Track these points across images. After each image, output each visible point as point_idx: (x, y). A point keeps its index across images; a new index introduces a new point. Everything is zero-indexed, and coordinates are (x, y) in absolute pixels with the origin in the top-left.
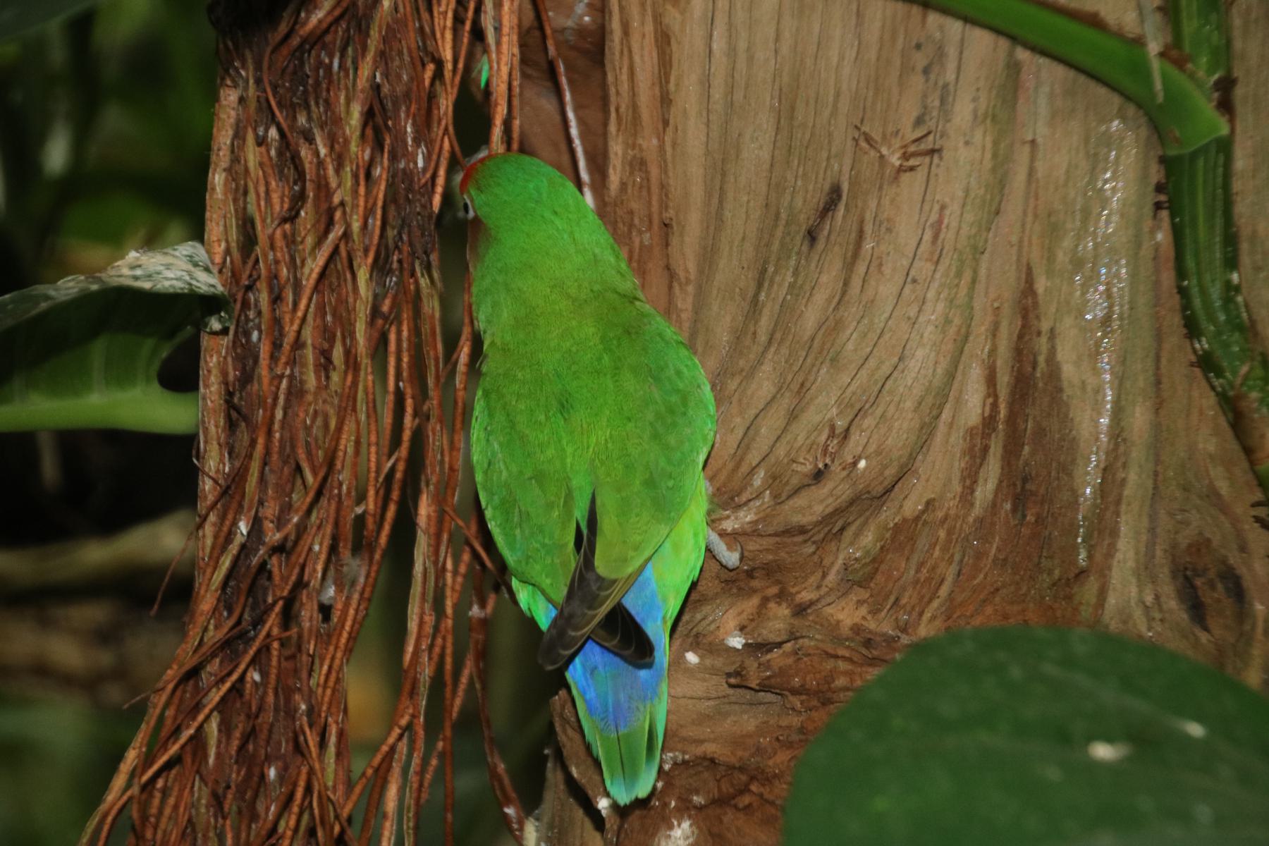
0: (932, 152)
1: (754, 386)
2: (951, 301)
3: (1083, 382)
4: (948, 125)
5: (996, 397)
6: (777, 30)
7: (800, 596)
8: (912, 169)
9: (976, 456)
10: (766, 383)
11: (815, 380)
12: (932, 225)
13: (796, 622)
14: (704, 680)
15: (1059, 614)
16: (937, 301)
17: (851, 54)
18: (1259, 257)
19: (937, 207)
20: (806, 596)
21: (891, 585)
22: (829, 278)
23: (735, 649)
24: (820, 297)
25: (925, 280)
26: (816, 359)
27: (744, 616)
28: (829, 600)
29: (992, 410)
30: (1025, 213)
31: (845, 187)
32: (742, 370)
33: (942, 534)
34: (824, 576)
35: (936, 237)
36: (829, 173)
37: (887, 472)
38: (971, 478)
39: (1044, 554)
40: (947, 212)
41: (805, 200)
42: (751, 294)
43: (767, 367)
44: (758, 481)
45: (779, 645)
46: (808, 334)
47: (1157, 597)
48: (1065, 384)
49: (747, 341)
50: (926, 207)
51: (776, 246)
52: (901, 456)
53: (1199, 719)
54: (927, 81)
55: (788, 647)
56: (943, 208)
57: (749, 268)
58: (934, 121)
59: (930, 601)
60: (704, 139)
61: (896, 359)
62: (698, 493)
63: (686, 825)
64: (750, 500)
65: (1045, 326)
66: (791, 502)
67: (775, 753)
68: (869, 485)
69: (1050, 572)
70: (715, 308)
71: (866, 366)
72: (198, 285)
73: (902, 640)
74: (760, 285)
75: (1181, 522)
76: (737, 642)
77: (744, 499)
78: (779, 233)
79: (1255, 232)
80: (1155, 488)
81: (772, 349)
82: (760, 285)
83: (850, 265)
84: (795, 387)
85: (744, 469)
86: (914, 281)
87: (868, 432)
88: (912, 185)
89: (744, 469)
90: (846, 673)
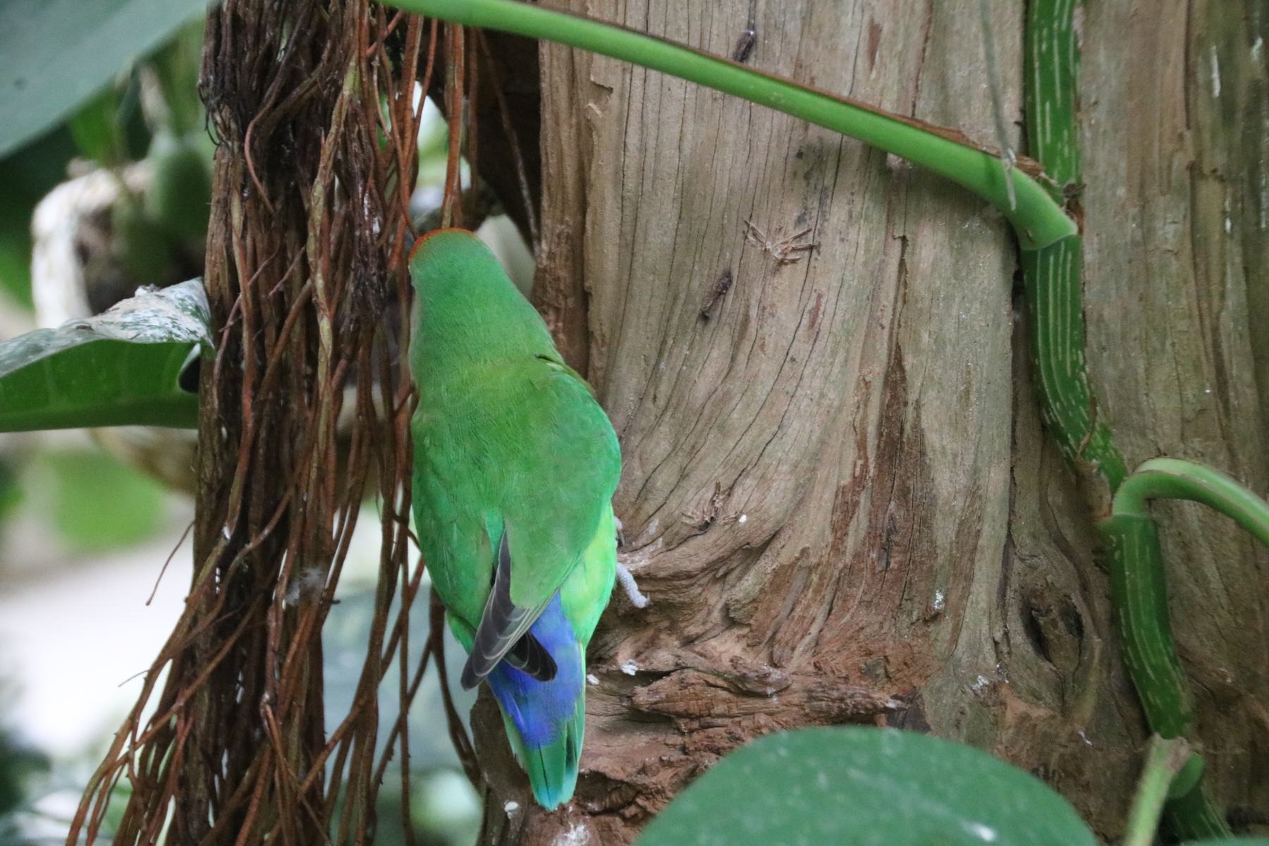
0: (811, 248)
1: (652, 445)
2: (826, 378)
3: (944, 448)
4: (826, 224)
5: (867, 459)
6: (681, 132)
7: (687, 629)
8: (794, 261)
9: (845, 509)
10: (663, 443)
11: (705, 442)
12: (810, 312)
13: (682, 653)
14: (603, 700)
15: (916, 650)
16: (812, 377)
17: (742, 157)
18: (1103, 338)
19: (814, 295)
20: (693, 630)
21: (769, 620)
22: (717, 355)
23: (628, 675)
24: (710, 371)
25: (802, 360)
26: (706, 425)
27: (640, 643)
28: (713, 633)
29: (862, 471)
30: (896, 299)
31: (735, 274)
32: (644, 429)
33: (815, 578)
34: (709, 613)
35: (812, 324)
36: (722, 260)
37: (765, 527)
38: (840, 530)
39: (905, 597)
40: (823, 300)
41: (699, 284)
42: (653, 362)
43: (664, 429)
44: (653, 527)
45: (668, 674)
46: (700, 402)
47: (1006, 634)
48: (929, 449)
49: (649, 404)
50: (805, 295)
51: (675, 321)
52: (777, 513)
53: (988, 823)
54: (808, 184)
55: (674, 676)
56: (820, 296)
57: (653, 339)
58: (814, 220)
59: (803, 637)
60: (619, 222)
61: (775, 428)
62: (609, 524)
63: (581, 828)
64: (645, 546)
65: (912, 397)
66: (680, 549)
67: (659, 771)
68: (749, 537)
69: (910, 614)
70: (624, 370)
71: (750, 433)
72: (179, 333)
73: (773, 675)
74: (660, 354)
75: (1030, 566)
76: (630, 669)
77: (640, 545)
78: (678, 311)
79: (1101, 316)
80: (1009, 535)
81: (669, 413)
82: (660, 354)
83: (736, 346)
84: (687, 448)
85: (643, 516)
86: (793, 360)
87: (750, 490)
88: (789, 278)
89: (643, 516)
90: (724, 701)
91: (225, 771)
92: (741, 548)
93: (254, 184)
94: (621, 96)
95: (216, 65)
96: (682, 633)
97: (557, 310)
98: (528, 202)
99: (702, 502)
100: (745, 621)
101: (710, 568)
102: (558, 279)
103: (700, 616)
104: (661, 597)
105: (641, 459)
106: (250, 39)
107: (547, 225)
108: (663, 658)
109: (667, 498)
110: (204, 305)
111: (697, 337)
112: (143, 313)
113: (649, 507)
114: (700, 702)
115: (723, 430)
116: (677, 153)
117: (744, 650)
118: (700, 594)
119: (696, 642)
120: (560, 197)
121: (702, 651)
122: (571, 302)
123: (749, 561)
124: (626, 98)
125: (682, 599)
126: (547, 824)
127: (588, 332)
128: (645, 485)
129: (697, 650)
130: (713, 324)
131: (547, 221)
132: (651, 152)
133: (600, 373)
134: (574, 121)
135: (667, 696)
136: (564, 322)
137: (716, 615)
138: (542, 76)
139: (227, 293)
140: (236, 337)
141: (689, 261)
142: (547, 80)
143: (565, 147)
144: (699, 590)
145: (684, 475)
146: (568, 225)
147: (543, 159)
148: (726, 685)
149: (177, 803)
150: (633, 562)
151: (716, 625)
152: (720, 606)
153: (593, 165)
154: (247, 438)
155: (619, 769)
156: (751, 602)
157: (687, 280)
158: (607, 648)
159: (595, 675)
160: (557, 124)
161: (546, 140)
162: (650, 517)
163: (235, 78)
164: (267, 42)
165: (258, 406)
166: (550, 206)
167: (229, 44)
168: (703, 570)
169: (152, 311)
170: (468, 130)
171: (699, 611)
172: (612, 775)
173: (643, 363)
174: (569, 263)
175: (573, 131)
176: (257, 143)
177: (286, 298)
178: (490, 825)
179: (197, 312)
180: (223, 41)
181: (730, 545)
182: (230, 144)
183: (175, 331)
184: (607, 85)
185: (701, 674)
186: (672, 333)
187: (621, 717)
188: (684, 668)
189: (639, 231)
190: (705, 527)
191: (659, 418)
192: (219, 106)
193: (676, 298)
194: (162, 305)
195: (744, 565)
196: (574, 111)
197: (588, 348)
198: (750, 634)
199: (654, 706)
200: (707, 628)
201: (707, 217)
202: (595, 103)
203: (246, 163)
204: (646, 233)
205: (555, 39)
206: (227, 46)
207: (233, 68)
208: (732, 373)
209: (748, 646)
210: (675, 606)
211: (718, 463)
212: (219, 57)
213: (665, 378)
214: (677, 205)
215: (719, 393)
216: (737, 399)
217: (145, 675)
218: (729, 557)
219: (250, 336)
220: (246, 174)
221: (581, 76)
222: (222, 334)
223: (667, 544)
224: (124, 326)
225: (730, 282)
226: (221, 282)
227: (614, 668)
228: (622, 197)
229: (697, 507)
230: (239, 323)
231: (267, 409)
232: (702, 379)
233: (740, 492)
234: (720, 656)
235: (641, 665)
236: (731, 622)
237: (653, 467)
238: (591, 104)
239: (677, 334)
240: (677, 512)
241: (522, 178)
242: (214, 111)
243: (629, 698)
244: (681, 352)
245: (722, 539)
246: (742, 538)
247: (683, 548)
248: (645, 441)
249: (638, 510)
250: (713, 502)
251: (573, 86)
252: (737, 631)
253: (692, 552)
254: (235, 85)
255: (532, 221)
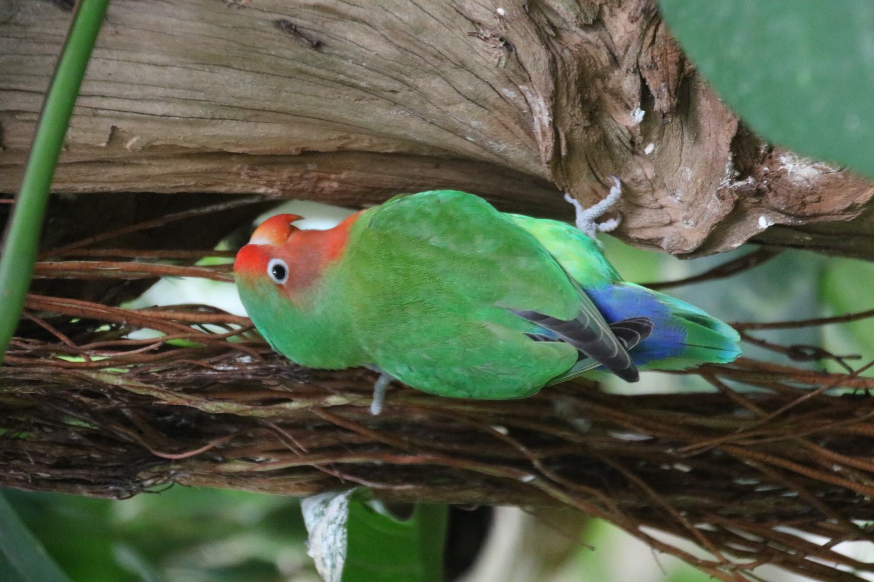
1: (435, 94)
7: (604, 62)
11: (431, 46)
13: (624, 68)
14: (668, 140)
20: (604, 57)
22: (352, 34)
23: (645, 117)
24: (366, 40)
27: (617, 106)
28: (608, 39)
31: (277, 17)
32: (422, 102)
34: (589, 42)
42: (360, 93)
43: (421, 83)
44: (509, 93)
45: (643, 81)
46: (394, 50)
49: (399, 96)
51: (322, 72)
55: (646, 74)
57: (340, 93)
60: (234, 122)
63: (783, 159)
64: (526, 101)
66: (529, 70)
70: (369, 119)
72: (340, 518)
74: (353, 86)
76: (639, 115)
78: (313, 70)
81: (406, 79)
82: (353, 86)
83: (342, 17)
84: (437, 63)
85: (501, 103)
91: (752, 482)
92: (528, 14)
93: (210, 450)
94: (119, 118)
95: (99, 483)
96: (607, 68)
97: (320, 179)
98: (230, 204)
99: (486, 49)
100: (597, 9)
101: (546, 42)
102: (291, 179)
103: (592, 51)
104: (573, 87)
105: (449, 105)
106: (79, 453)
107: (243, 187)
108: (629, 85)
109: (483, 80)
110: (323, 497)
111: (337, 52)
112: (325, 551)
113: (492, 97)
114: (669, 51)
115: (420, 29)
116: (168, 68)
117: (623, 10)
118: (570, 51)
119: (616, 54)
120: (215, 176)
121: (624, 49)
122: (311, 167)
123: (540, 6)
124: (120, 114)
125: (575, 68)
126: (779, 190)
127: (338, 151)
128: (473, 102)
129: (622, 54)
130: (323, 38)
131: (238, 188)
132: (169, 92)
133: (375, 141)
134: (145, 162)
135: (663, 81)
136: (330, 173)
137: (592, 36)
138: (105, 190)
139: (313, 476)
140: (354, 469)
141: (267, 59)
142: (108, 186)
143: (169, 170)
144: (567, 52)
145: (462, 65)
146: (241, 168)
147: (182, 190)
148: (653, 28)
149: (779, 524)
150: (541, 113)
151: (600, 37)
152: (582, 33)
153: (184, 145)
154: (442, 461)
155: (728, 125)
156: (579, 4)
157: (285, 62)
158: (621, 135)
159: (645, 147)
160: (148, 177)
161: (164, 187)
162: (501, 96)
163: (111, 467)
164: (81, 438)
165: (413, 450)
166: (225, 185)
167: (81, 472)
168: (548, 48)
169: (323, 542)
170: (162, 259)
171: (586, 51)
172: (734, 132)
173: (361, 102)
174: (276, 168)
175: (154, 163)
176: (174, 448)
177: (319, 424)
178: (793, 242)
179: (326, 503)
180: (76, 477)
181: (525, 23)
182: (172, 472)
183: (338, 521)
184: (110, 131)
185: (644, 50)
186: (332, 75)
187: (684, 123)
188: (638, 66)
189: (242, 105)
190: (508, 46)
191: (411, 87)
192: (138, 482)
193: (301, 71)
194: (318, 534)
195: (545, 11)
196: (136, 162)
197: (353, 152)
198: (609, 5)
199: (673, 93)
200: (602, 44)
201: (226, 43)
202: (127, 142)
203: (191, 458)
204: (242, 98)
205: (50, 178)
206: (82, 474)
207: (102, 468)
208: (368, 21)
209: (620, 6)
210: (582, 74)
211: (451, 34)
212: (92, 480)
213: (375, 82)
214: (216, 69)
215: (386, 32)
216: (391, 16)
217: (657, 552)
218: (536, 24)
219: (350, 455)
220: (200, 458)
221: (103, 155)
222: (346, 481)
223: (524, 81)
224: (334, 566)
225: (284, 21)
226: (303, 482)
227: (638, 130)
228: (213, 119)
229: (490, 54)
230: (338, 466)
231: (417, 442)
232: (374, 49)
233: (476, 14)
234: (628, 33)
235: (635, 104)
236: (598, 23)
237: (455, 95)
238: (128, 146)
239: (334, 71)
240: (496, 72)
241: (208, 209)
242: (142, 486)
243: (664, 116)
244: (350, 68)
245: (519, 30)
246: (518, 13)
247: (528, 66)
248: (432, 101)
249: (496, 108)
250: (486, 39)
251: (113, 162)
252: (606, 18)
253: (531, 59)
254: (117, 467)
255: (247, 201)
